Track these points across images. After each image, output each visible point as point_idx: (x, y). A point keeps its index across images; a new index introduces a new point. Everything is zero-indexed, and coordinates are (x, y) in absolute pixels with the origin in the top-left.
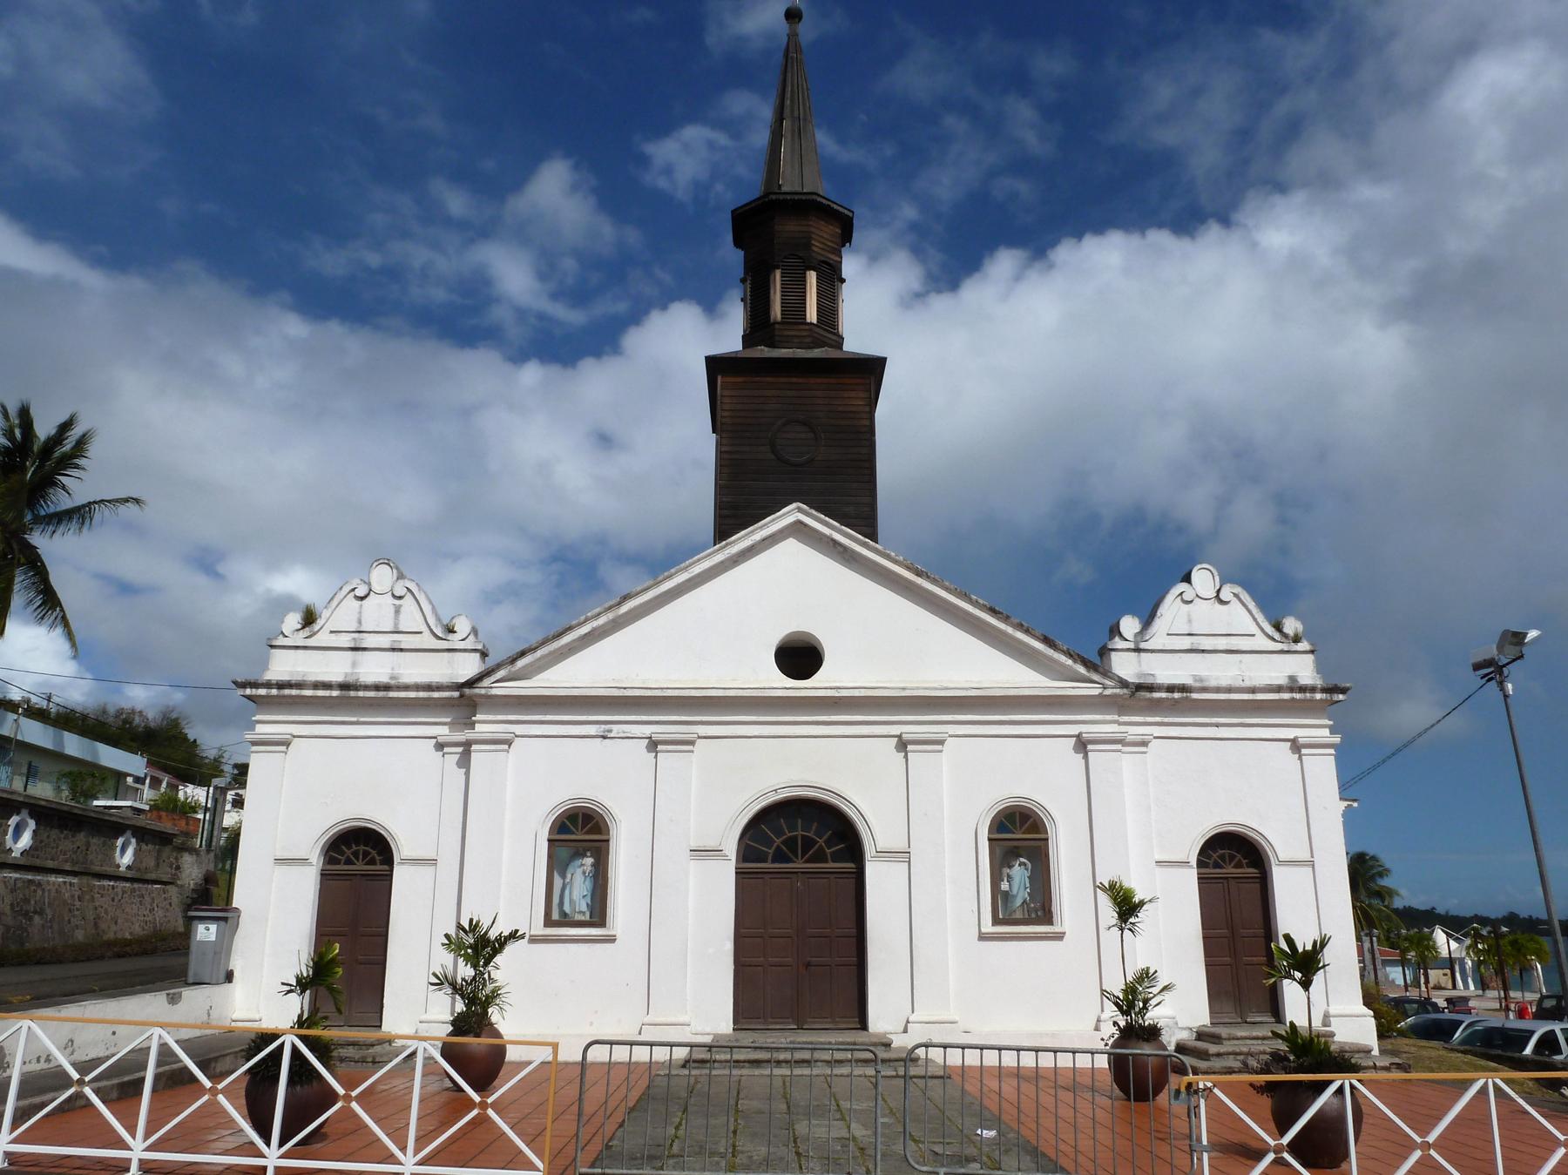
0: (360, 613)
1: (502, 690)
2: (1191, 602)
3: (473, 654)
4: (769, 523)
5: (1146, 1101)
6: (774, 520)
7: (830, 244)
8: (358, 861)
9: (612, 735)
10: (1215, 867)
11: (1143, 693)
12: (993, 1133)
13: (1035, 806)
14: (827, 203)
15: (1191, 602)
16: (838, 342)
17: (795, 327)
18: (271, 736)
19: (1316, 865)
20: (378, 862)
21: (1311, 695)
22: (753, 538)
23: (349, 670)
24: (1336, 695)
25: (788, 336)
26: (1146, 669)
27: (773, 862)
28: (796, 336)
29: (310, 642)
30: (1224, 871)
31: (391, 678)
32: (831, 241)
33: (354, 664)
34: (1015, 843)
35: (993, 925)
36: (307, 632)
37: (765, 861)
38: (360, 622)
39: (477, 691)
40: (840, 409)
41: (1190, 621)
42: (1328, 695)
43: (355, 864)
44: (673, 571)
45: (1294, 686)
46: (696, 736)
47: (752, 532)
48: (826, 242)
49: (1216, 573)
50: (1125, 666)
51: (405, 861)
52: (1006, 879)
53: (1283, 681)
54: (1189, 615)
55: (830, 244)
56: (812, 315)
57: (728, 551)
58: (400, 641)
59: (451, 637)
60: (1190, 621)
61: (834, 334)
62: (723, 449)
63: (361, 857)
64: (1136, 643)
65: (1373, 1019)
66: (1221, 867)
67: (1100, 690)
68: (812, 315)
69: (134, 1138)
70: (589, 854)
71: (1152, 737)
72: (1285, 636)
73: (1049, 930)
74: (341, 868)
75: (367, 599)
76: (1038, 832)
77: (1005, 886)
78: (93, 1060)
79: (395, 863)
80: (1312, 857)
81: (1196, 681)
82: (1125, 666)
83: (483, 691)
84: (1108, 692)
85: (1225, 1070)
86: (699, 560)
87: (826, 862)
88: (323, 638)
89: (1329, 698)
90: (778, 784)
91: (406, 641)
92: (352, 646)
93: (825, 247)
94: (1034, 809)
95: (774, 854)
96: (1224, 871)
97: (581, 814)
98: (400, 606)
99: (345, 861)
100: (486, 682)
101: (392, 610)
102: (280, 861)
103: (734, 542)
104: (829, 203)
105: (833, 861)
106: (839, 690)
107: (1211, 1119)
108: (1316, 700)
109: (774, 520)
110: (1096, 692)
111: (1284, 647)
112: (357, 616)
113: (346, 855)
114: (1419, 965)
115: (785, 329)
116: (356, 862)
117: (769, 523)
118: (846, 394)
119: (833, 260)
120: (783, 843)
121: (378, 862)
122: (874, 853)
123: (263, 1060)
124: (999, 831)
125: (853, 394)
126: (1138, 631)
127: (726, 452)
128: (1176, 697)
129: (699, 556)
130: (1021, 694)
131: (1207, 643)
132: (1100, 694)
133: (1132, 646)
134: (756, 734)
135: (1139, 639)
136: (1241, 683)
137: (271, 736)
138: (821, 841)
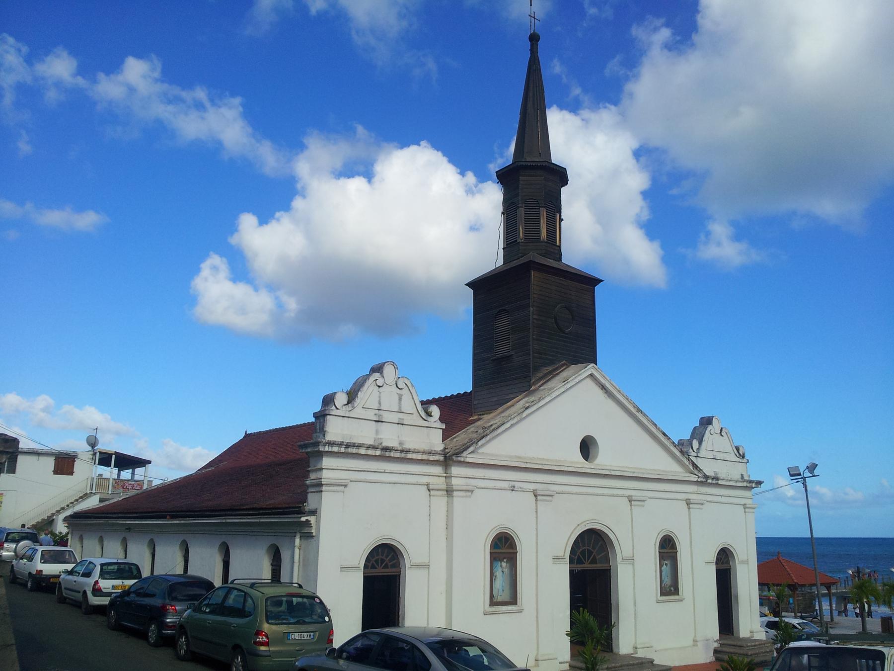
0: (380, 397)
2: (401, 389)
3: (439, 430)
12: (857, 660)
13: (507, 530)
15: (401, 389)
16: (558, 255)
19: (635, 565)
20: (389, 567)
33: (377, 432)
36: (349, 407)
39: (459, 459)
43: (376, 568)
46: (555, 492)
56: (544, 234)
59: (429, 419)
62: (534, 317)
68: (544, 234)
71: (475, 487)
74: (368, 572)
76: (512, 548)
79: (407, 568)
80: (633, 557)
83: (462, 459)
84: (699, 480)
85: (722, 653)
88: (358, 412)
95: (577, 559)
99: (372, 566)
100: (464, 454)
101: (397, 397)
112: (378, 399)
113: (371, 563)
114: (885, 596)
116: (377, 566)
122: (621, 560)
127: (536, 319)
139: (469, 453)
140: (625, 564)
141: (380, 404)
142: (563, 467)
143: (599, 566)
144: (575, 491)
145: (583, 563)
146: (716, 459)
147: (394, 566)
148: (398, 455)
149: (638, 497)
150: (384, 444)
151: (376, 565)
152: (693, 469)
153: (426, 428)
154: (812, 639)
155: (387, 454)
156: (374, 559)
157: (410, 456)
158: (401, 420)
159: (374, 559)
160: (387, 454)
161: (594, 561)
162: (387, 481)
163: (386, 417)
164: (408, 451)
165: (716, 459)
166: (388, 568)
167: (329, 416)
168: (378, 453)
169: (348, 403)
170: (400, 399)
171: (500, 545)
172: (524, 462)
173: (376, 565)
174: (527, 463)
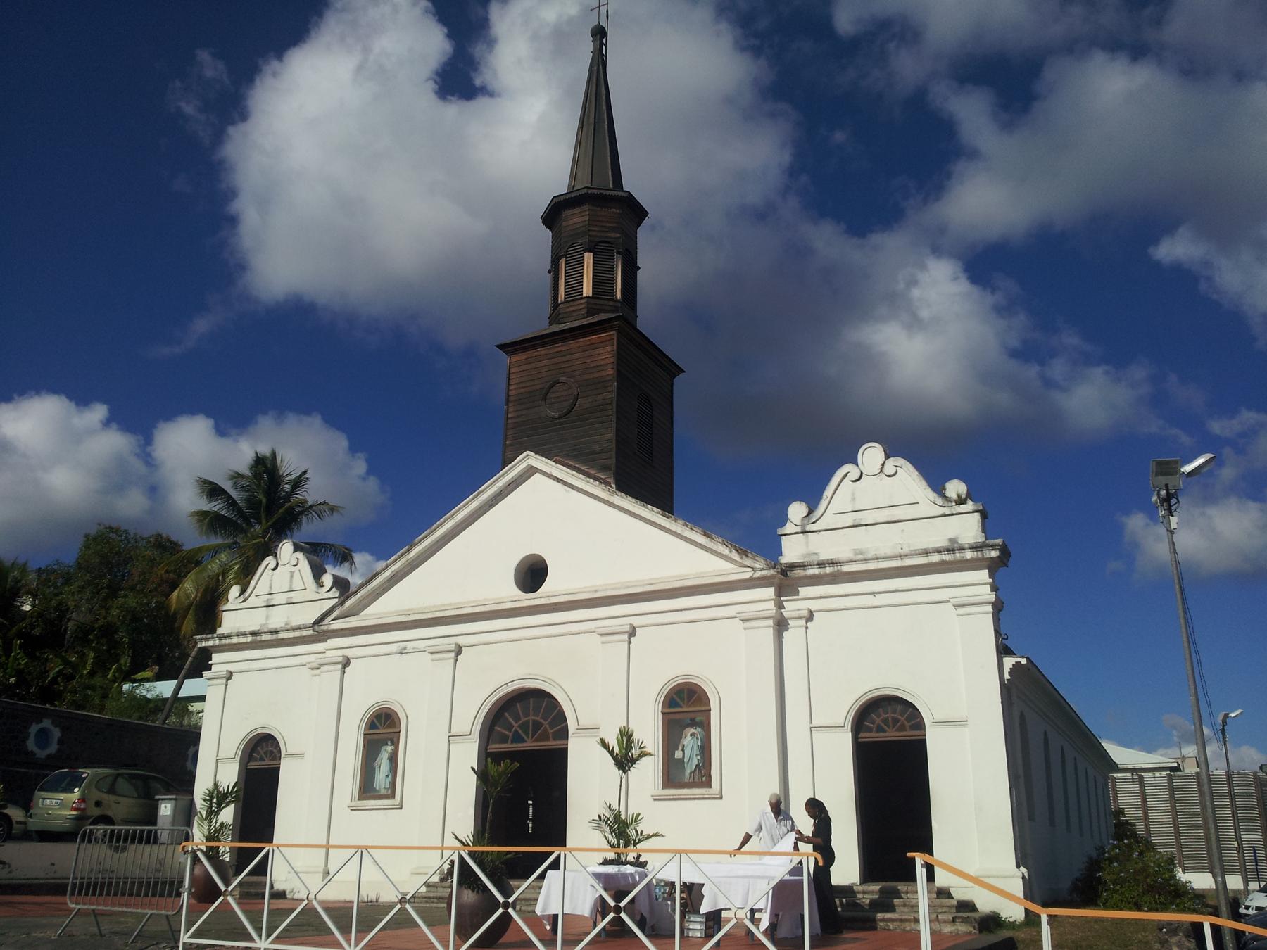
0: (271, 580)
4: (508, 471)
6: (511, 468)
7: (608, 225)
8: (893, 728)
9: (406, 651)
11: (798, 571)
14: (599, 192)
20: (908, 728)
21: (962, 555)
24: (987, 552)
25: (569, 312)
26: (812, 549)
27: (512, 742)
28: (574, 311)
31: (286, 624)
33: (267, 618)
34: (376, 737)
36: (242, 598)
37: (506, 742)
38: (271, 587)
39: (322, 628)
40: (592, 365)
41: (853, 499)
42: (979, 553)
44: (442, 520)
45: (953, 547)
47: (496, 480)
48: (604, 224)
49: (865, 446)
52: (680, 748)
54: (853, 494)
55: (608, 225)
57: (480, 498)
58: (291, 598)
60: (853, 499)
63: (885, 727)
64: (803, 526)
66: (885, 731)
67: (751, 574)
69: (256, 942)
70: (389, 743)
72: (948, 499)
73: (675, 793)
75: (896, 476)
77: (678, 754)
81: (805, 558)
82: (792, 551)
84: (758, 574)
86: (460, 509)
88: (252, 601)
90: (536, 675)
91: (296, 597)
92: (265, 605)
96: (887, 734)
97: (674, 696)
98: (294, 572)
100: (327, 621)
104: (602, 191)
109: (511, 468)
110: (747, 576)
111: (947, 511)
117: (508, 471)
118: (596, 352)
119: (611, 238)
121: (908, 728)
124: (670, 706)
125: (601, 351)
126: (805, 515)
128: (828, 572)
129: (459, 506)
130: (504, 608)
133: (799, 529)
134: (919, 600)
135: (806, 522)
136: (900, 550)
140: (582, 737)
142: (465, 609)
143: (551, 744)
146: (293, 603)
147: (274, 759)
148: (268, 637)
149: (611, 628)
152: (742, 558)
154: (1145, 909)
156: (893, 715)
157: (281, 636)
159: (893, 715)
160: (258, 638)
161: (544, 737)
163: (277, 599)
164: (277, 632)
165: (293, 603)
166: (906, 730)
167: (783, 537)
168: (249, 639)
170: (292, 577)
174: (409, 614)
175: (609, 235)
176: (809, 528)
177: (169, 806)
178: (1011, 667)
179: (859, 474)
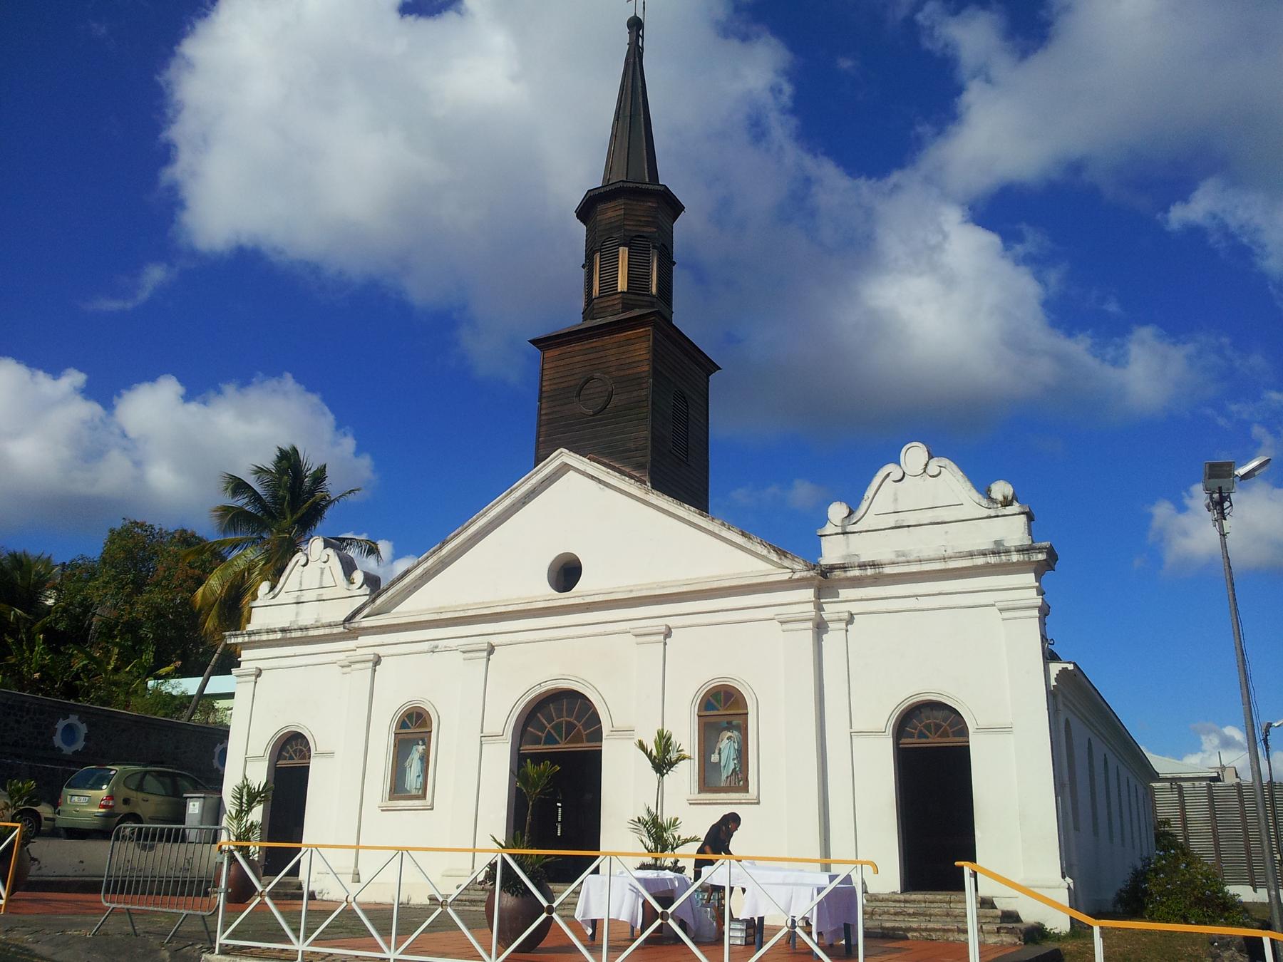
1: (367, 623)
5: (96, 893)
6: (545, 466)
9: (437, 650)
10: (919, 737)
13: (706, 687)
17: (609, 298)
18: (797, 615)
22: (531, 482)
23: (293, 619)
26: (853, 550)
27: (545, 744)
29: (273, 602)
30: (927, 741)
32: (644, 216)
35: (699, 793)
36: (271, 595)
39: (353, 625)
40: (627, 361)
50: (832, 551)
51: (979, 730)
52: (717, 751)
53: (990, 546)
54: (895, 494)
58: (322, 594)
60: (896, 500)
61: (648, 295)
65: (1067, 890)
67: (790, 575)
77: (715, 758)
78: (332, 901)
82: (832, 551)
83: (356, 625)
84: (797, 576)
86: (493, 506)
87: (582, 742)
89: (1027, 559)
91: (327, 593)
93: (639, 223)
94: (708, 688)
96: (930, 740)
100: (358, 618)
102: (1007, 729)
103: (514, 489)
105: (588, 741)
106: (585, 598)
107: (98, 902)
108: (1013, 563)
109: (545, 466)
110: (786, 577)
111: (992, 513)
112: (300, 579)
115: (602, 302)
116: (563, 739)
118: (632, 348)
119: (643, 232)
120: (552, 727)
123: (8, 872)
124: (706, 709)
125: (637, 347)
126: (846, 515)
128: (869, 574)
131: (911, 519)
132: (790, 578)
133: (839, 530)
137: (797, 615)
138: (579, 726)
139: (364, 618)
141: (301, 584)
143: (584, 746)
144: (603, 631)
145: (556, 742)
148: (299, 634)
150: (863, 560)
151: (294, 755)
152: (780, 559)
153: (921, 523)
155: (288, 635)
158: (320, 596)
160: (288, 635)
161: (578, 739)
162: (680, 624)
166: (949, 737)
168: (279, 636)
169: (270, 592)
170: (322, 573)
171: (410, 725)
172: (438, 613)
173: (294, 755)
175: (646, 229)
176: (849, 529)
177: (197, 804)
178: (1058, 673)
179: (902, 474)
